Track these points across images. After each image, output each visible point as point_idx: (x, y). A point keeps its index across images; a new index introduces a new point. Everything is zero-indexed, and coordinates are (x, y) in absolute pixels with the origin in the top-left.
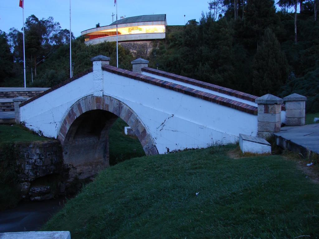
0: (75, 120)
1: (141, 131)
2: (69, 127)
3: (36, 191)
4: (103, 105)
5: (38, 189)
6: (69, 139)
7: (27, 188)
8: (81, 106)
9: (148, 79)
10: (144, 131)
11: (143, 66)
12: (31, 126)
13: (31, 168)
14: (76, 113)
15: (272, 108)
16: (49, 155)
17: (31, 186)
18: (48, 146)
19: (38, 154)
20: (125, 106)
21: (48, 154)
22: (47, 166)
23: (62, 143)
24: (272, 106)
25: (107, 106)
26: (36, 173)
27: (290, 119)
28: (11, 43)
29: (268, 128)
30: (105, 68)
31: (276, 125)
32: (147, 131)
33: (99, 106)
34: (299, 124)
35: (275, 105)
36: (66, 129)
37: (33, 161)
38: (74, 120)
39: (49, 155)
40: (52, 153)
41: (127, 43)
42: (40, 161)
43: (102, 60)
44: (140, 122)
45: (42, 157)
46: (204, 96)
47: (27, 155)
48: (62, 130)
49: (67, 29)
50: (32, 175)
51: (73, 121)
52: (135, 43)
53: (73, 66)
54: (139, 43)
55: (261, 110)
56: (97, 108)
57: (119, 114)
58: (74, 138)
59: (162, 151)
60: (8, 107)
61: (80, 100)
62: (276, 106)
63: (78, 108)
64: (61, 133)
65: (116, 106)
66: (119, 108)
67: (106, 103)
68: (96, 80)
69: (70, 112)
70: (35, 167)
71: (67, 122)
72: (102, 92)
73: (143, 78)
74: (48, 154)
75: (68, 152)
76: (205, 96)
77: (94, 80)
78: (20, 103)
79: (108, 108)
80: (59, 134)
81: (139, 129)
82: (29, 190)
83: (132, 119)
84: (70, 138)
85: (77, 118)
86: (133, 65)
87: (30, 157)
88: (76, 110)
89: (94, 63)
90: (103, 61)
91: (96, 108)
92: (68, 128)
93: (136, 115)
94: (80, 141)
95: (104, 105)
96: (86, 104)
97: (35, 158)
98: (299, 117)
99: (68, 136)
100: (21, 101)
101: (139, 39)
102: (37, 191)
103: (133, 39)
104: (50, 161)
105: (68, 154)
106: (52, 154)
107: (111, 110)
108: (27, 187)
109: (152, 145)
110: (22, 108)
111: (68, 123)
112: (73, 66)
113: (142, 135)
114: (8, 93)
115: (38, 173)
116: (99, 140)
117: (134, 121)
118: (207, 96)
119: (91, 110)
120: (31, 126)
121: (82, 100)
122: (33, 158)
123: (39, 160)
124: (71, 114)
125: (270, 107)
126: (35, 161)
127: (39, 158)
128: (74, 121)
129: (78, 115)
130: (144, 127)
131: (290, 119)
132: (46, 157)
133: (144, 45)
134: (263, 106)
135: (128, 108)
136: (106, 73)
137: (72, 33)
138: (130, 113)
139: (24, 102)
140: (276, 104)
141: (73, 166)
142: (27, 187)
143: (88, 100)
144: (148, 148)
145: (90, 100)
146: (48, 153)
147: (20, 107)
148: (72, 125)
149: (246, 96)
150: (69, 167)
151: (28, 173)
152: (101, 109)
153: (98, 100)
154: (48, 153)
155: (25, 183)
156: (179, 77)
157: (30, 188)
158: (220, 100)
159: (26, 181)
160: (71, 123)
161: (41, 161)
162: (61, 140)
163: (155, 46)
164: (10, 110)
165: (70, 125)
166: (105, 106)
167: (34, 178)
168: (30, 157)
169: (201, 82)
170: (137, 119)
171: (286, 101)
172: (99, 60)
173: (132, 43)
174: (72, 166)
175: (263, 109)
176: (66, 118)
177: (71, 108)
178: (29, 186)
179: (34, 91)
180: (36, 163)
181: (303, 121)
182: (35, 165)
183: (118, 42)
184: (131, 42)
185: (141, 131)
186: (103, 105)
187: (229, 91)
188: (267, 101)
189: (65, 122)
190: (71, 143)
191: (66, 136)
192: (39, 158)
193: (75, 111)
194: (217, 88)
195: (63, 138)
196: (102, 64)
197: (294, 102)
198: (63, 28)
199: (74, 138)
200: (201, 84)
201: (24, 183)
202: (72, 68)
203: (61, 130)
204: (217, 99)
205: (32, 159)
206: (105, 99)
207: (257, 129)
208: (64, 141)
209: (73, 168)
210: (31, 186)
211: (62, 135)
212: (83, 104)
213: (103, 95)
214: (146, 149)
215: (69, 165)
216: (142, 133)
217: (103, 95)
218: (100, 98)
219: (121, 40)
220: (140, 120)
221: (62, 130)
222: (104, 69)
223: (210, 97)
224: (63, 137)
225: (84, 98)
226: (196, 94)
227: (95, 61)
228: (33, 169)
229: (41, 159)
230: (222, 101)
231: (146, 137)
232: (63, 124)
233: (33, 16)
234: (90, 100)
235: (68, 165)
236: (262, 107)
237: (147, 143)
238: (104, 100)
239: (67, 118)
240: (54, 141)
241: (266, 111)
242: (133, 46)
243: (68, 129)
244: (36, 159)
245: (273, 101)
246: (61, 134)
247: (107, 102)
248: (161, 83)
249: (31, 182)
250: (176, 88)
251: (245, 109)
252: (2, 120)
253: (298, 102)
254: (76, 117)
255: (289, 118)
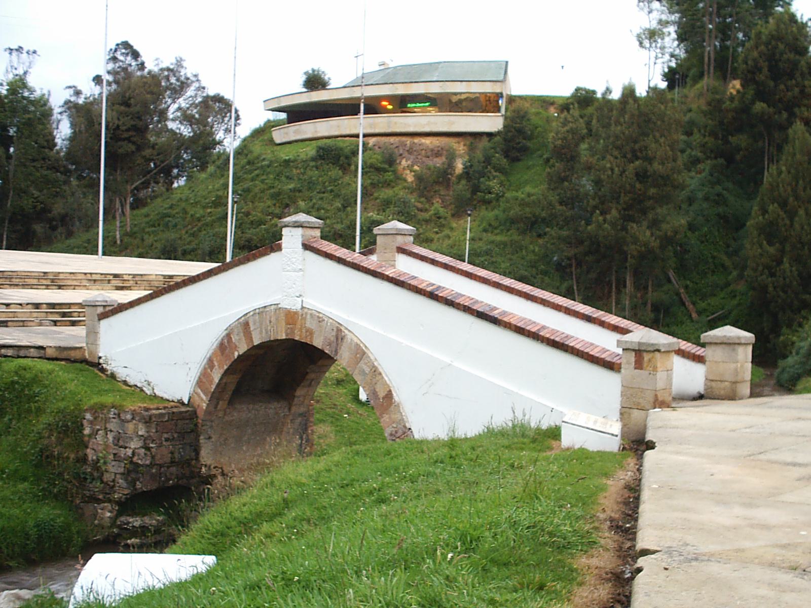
0: (236, 360)
1: (381, 394)
2: (219, 376)
3: (131, 525)
4: (301, 330)
5: (137, 521)
6: (218, 403)
7: (109, 517)
8: (252, 329)
9: (402, 279)
10: (389, 395)
11: (400, 240)
12: (126, 367)
13: (121, 470)
14: (237, 344)
15: (650, 361)
16: (167, 440)
17: (120, 513)
18: (166, 418)
19: (142, 436)
20: (349, 336)
21: (165, 438)
22: (161, 466)
23: (201, 414)
24: (651, 355)
25: (310, 332)
26: (133, 483)
27: (714, 384)
28: (63, 130)
29: (641, 401)
30: (310, 246)
31: (656, 395)
32: (395, 395)
33: (292, 330)
34: (732, 397)
35: (656, 353)
36: (211, 382)
37: (129, 452)
38: (233, 360)
39: (167, 440)
40: (176, 435)
41: (392, 139)
42: (145, 454)
43: (302, 227)
44: (380, 374)
45: (151, 445)
46: (516, 326)
47: (114, 438)
48: (201, 383)
49: (225, 97)
50: (125, 485)
51: (229, 363)
52: (417, 140)
53: (236, 202)
54: (427, 141)
55: (628, 363)
56: (287, 335)
57: (336, 352)
58: (231, 403)
59: (417, 436)
60: (64, 315)
61: (248, 315)
62: (657, 354)
63: (244, 332)
64: (200, 388)
65: (332, 336)
66: (337, 339)
67: (308, 325)
68: (288, 271)
69: (222, 340)
70: (132, 470)
71: (216, 364)
72: (299, 300)
73: (391, 275)
74: (165, 438)
75: (212, 436)
76: (519, 325)
77: (284, 270)
78: (100, 310)
79: (311, 338)
80: (194, 391)
81: (377, 390)
82: (115, 522)
83: (365, 367)
84: (221, 402)
85: (239, 356)
86: (378, 238)
87: (121, 443)
88: (237, 338)
89: (285, 231)
90: (305, 229)
91: (284, 337)
92: (216, 376)
93: (372, 358)
94: (244, 412)
95: (304, 331)
96: (261, 324)
97: (133, 445)
98: (733, 380)
99: (215, 398)
100: (104, 306)
101: (427, 129)
102: (133, 527)
103: (411, 129)
104: (170, 455)
105: (213, 440)
106: (174, 438)
107: (318, 343)
108: (109, 514)
109: (405, 427)
110: (104, 323)
111: (217, 367)
112: (236, 202)
113: (382, 405)
114: (61, 276)
115: (138, 483)
116: (290, 409)
117: (367, 370)
118: (523, 326)
119: (272, 339)
120: (126, 367)
121: (255, 314)
122: (127, 445)
123: (143, 450)
124: (224, 346)
125: (646, 357)
126: (134, 454)
127: (142, 447)
128: (233, 362)
129: (243, 348)
130: (389, 386)
131: (714, 384)
132: (160, 445)
133: (440, 149)
134: (633, 354)
135: (355, 340)
136: (309, 254)
137: (236, 111)
138: (360, 353)
139: (111, 308)
140: (659, 351)
141: (223, 471)
142: (109, 514)
143: (268, 317)
144: (396, 432)
145: (271, 317)
146: (166, 436)
147: (100, 320)
148: (226, 373)
149: (622, 326)
150: (214, 472)
151: (114, 481)
152: (297, 338)
153: (291, 317)
154: (166, 436)
155: (106, 504)
156: (479, 274)
157: (117, 517)
158: (548, 336)
159: (110, 501)
160: (226, 367)
161: (149, 453)
162: (198, 406)
163: (471, 149)
164: (68, 323)
165: (222, 371)
166: (306, 332)
167: (127, 494)
168: (121, 443)
169: (526, 288)
170: (374, 366)
171: (708, 343)
172: (298, 227)
173: (408, 141)
174: (220, 470)
175: (633, 359)
176: (213, 353)
177: (226, 332)
178: (115, 513)
179: (129, 275)
180: (135, 459)
181: (746, 389)
182: (131, 462)
183: (365, 136)
184: (404, 139)
185: (381, 394)
186: (301, 330)
187: (586, 313)
188: (640, 344)
189: (210, 363)
190: (221, 414)
191: (211, 397)
192: (142, 447)
193: (234, 338)
194: (560, 304)
195: (203, 402)
196: (303, 236)
197: (724, 346)
198: (211, 92)
199: (231, 403)
200: (528, 292)
201: (102, 505)
202: (233, 207)
203: (200, 383)
204: (459, 300)
205: (126, 448)
206: (306, 318)
207: (619, 403)
208: (204, 408)
209: (223, 474)
210: (120, 513)
211: (202, 395)
212: (255, 324)
213: (303, 308)
214: (391, 435)
215: (214, 468)
216: (383, 398)
217: (303, 308)
218: (296, 313)
219: (377, 131)
220: (381, 370)
221: (201, 382)
222: (306, 247)
223: (528, 328)
224: (202, 400)
225: (257, 311)
226: (501, 320)
227: (288, 226)
228: (126, 474)
229: (148, 449)
230: (552, 338)
231: (393, 407)
232: (205, 369)
233: (126, 45)
234: (271, 317)
235: (212, 467)
236: (632, 357)
237: (394, 422)
238: (305, 319)
239: (214, 354)
240: (183, 409)
241: (639, 365)
242: (410, 152)
243: (217, 380)
244: (135, 449)
245: (653, 345)
246: (199, 391)
247: (310, 324)
248: (429, 289)
249: (119, 503)
250: (459, 304)
251: (597, 358)
252: (54, 350)
253: (732, 346)
254: (236, 354)
255: (712, 381)
